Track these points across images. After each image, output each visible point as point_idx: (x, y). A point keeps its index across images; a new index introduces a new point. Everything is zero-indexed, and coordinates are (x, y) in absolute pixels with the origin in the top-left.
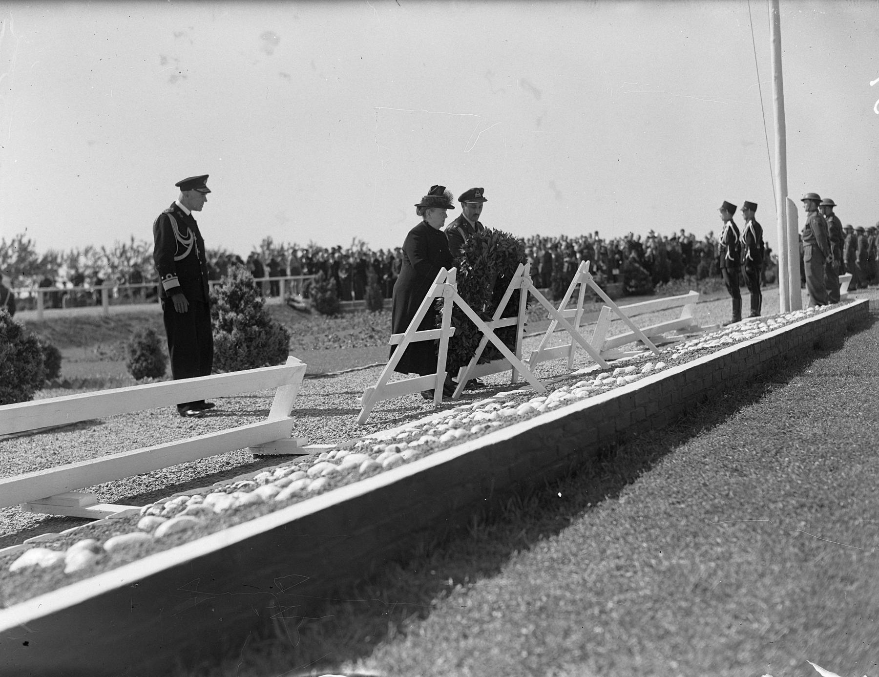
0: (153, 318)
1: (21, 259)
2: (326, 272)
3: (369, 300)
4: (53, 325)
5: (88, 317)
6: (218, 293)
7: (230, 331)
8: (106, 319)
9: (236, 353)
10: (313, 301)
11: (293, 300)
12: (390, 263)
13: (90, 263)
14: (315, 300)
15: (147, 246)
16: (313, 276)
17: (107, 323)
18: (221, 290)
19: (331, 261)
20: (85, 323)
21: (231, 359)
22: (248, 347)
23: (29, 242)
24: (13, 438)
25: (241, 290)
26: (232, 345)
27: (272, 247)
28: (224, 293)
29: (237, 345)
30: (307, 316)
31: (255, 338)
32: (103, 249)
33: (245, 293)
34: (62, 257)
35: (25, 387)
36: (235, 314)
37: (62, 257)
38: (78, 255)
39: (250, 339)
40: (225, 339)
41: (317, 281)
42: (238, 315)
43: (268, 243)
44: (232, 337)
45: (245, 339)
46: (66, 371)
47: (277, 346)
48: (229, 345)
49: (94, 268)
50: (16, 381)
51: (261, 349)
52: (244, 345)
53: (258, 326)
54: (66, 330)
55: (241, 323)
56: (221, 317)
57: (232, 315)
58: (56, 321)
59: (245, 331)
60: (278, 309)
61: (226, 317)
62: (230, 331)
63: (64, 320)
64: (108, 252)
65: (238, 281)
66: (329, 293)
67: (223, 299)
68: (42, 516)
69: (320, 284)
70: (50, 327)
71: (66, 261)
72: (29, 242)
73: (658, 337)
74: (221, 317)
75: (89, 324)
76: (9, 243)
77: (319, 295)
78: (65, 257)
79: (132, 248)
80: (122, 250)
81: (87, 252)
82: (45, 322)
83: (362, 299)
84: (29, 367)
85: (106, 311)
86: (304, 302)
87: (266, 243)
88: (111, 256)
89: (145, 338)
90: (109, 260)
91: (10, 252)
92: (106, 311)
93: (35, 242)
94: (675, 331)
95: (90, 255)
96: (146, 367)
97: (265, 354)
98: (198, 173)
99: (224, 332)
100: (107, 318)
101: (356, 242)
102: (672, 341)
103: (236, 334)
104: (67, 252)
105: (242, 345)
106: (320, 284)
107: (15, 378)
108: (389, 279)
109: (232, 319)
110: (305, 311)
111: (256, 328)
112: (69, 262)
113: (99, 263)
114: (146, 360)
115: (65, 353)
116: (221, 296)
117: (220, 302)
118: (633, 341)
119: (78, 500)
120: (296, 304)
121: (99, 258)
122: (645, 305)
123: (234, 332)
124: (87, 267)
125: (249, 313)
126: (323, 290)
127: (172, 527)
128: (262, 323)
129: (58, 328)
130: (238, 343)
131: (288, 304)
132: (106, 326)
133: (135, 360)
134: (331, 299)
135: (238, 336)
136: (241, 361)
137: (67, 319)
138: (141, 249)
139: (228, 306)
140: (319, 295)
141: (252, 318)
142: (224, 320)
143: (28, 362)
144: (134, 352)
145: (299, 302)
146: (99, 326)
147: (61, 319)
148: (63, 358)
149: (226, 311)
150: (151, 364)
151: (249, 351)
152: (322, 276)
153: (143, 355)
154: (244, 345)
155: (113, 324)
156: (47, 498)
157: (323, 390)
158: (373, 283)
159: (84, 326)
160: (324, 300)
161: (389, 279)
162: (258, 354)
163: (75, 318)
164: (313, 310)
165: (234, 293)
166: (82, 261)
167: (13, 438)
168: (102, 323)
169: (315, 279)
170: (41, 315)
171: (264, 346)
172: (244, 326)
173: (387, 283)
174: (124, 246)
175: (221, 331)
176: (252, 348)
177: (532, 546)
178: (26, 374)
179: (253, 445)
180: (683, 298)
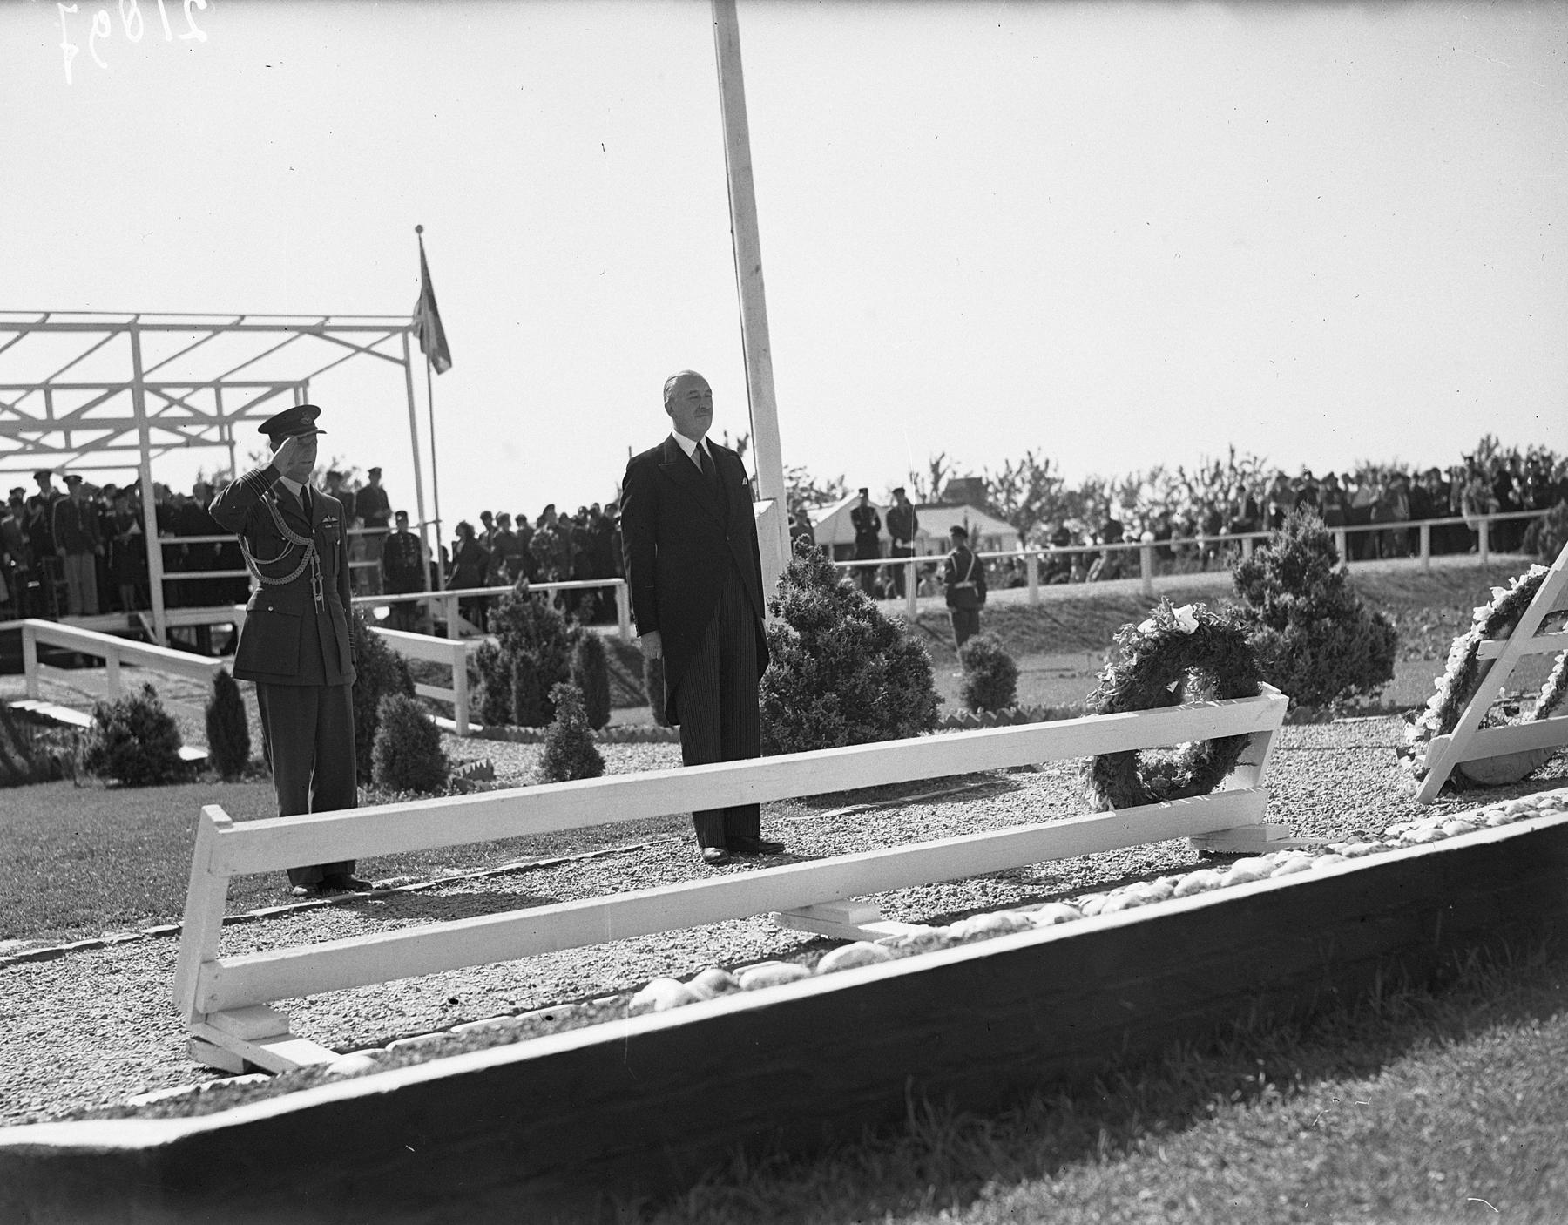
1: (1035, 495)
4: (1054, 611)
5: (1117, 598)
6: (1263, 559)
7: (1280, 627)
9: (1292, 667)
13: (1160, 497)
15: (1258, 463)
16: (1546, 512)
18: (1268, 554)
20: (1111, 608)
21: (1283, 676)
22: (1313, 655)
23: (1047, 463)
24: (872, 809)
25: (1303, 554)
26: (1283, 652)
27: (1497, 452)
28: (1274, 560)
29: (1293, 651)
31: (1326, 640)
32: (1181, 470)
33: (1309, 560)
34: (1112, 488)
35: (900, 726)
36: (1292, 597)
37: (1112, 488)
38: (1140, 484)
39: (1316, 643)
40: (1272, 640)
42: (1297, 598)
43: (1487, 446)
44: (1284, 638)
45: (1310, 641)
46: (1026, 693)
47: (1369, 654)
48: (1278, 652)
49: (1166, 505)
50: (887, 715)
51: (1337, 660)
52: (1307, 652)
53: (1332, 618)
54: (1077, 621)
55: (1303, 613)
56: (1267, 602)
57: (1287, 598)
58: (1059, 605)
59: (1308, 625)
60: (1475, 575)
61: (1276, 602)
62: (1280, 627)
63: (1074, 603)
65: (1299, 538)
67: (1272, 570)
68: (806, 937)
70: (1049, 616)
71: (1118, 494)
72: (1047, 463)
74: (1267, 602)
75: (1117, 609)
76: (1015, 467)
78: (1118, 488)
79: (1232, 467)
80: (1213, 471)
81: (1154, 477)
82: (1041, 607)
84: (909, 693)
85: (1148, 586)
88: (1193, 484)
90: (1191, 489)
91: (1018, 483)
92: (1148, 586)
95: (1158, 482)
97: (1344, 668)
99: (1271, 630)
100: (1149, 598)
103: (1291, 632)
105: (1302, 652)
107: (885, 713)
111: (1328, 621)
112: (1122, 496)
113: (1175, 495)
115: (1023, 664)
116: (1268, 565)
117: (1268, 575)
119: (846, 914)
121: (1174, 488)
123: (1289, 627)
124: (1155, 503)
125: (1316, 595)
127: (839, 959)
128: (1338, 613)
129: (1063, 618)
130: (1296, 649)
135: (1296, 634)
136: (1302, 680)
137: (1078, 600)
139: (1279, 582)
141: (1321, 603)
142: (1272, 605)
143: (906, 686)
147: (1069, 601)
148: (1019, 674)
149: (1277, 592)
151: (1315, 663)
154: (1307, 652)
156: (807, 907)
157: (1369, 741)
159: (1108, 614)
162: (1332, 668)
163: (1093, 598)
165: (1290, 560)
166: (1147, 494)
167: (872, 809)
168: (1139, 607)
169: (1550, 517)
170: (1035, 593)
171: (1342, 653)
172: (1307, 618)
175: (1266, 628)
176: (1320, 659)
177: (1470, 1035)
178: (902, 705)
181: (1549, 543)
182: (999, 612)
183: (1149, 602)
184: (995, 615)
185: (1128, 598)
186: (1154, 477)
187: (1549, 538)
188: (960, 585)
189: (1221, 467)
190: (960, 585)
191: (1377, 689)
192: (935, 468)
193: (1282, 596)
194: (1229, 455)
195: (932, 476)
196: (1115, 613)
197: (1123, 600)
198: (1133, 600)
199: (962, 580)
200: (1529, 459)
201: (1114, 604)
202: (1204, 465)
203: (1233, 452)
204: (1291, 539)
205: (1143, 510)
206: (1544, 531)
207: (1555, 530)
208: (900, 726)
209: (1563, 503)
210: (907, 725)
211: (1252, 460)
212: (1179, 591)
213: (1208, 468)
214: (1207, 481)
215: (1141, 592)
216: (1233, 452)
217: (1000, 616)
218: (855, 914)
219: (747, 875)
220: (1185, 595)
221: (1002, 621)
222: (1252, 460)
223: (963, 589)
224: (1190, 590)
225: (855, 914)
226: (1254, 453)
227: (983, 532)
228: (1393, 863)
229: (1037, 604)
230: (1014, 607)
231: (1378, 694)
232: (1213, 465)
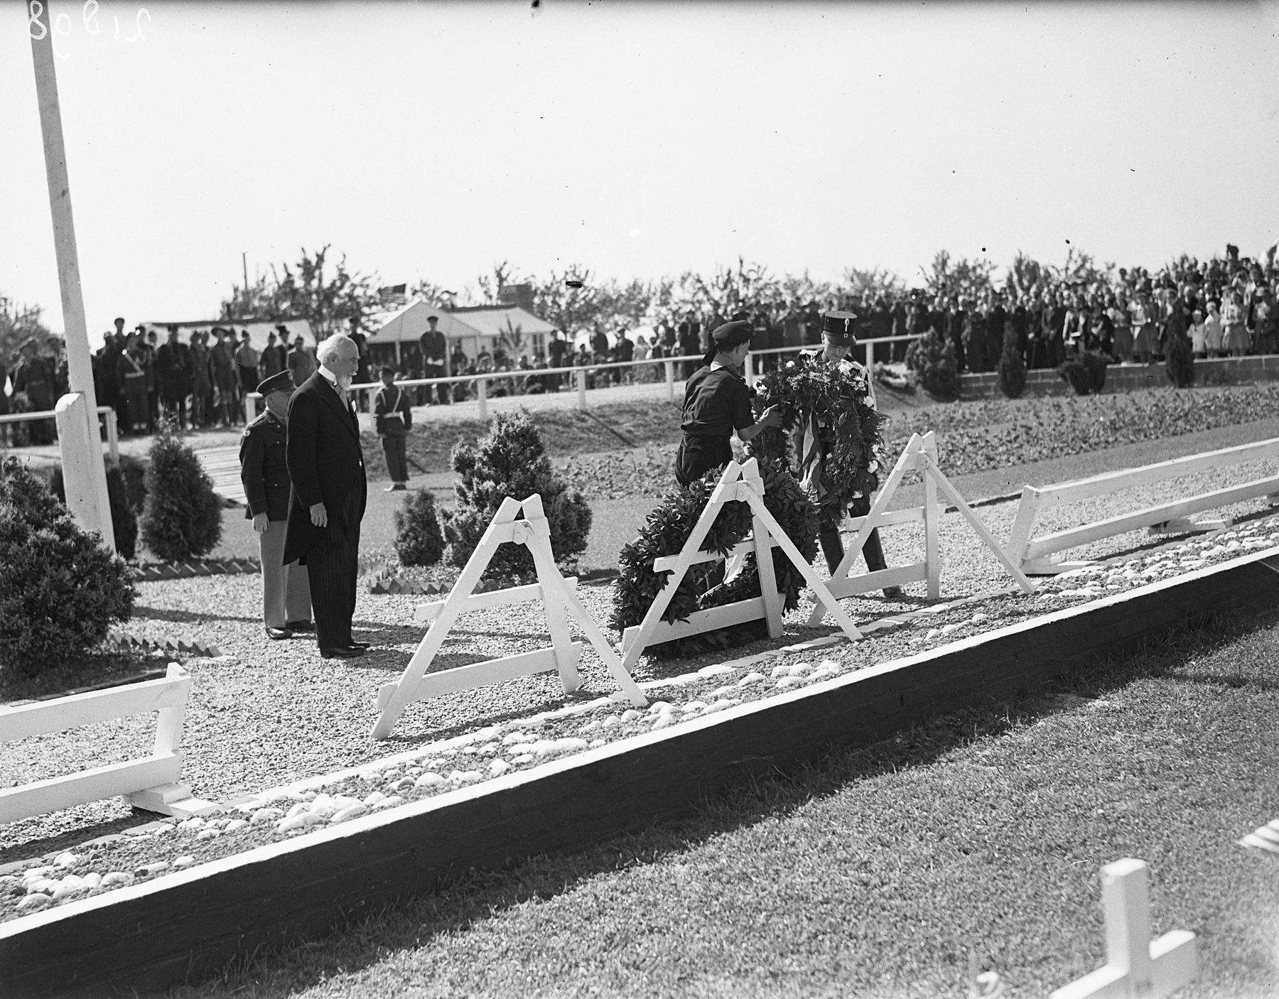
0: (655, 410)
2: (940, 331)
3: (1004, 373)
8: (582, 415)
10: (919, 375)
11: (889, 374)
12: (1039, 314)
13: (688, 297)
14: (922, 373)
15: (761, 270)
16: (919, 336)
17: (583, 420)
19: (953, 311)
20: (549, 422)
25: (505, 446)
30: (908, 398)
35: (84, 624)
41: (925, 343)
56: (475, 488)
64: (707, 282)
66: (943, 361)
69: (930, 348)
73: (1182, 521)
75: (555, 422)
76: (560, 276)
77: (928, 365)
80: (726, 278)
81: (684, 279)
83: (992, 370)
86: (906, 376)
87: (940, 260)
88: (709, 288)
89: (417, 505)
93: (595, 273)
94: (1265, 498)
96: (415, 548)
98: (268, 335)
101: (1075, 256)
102: (1202, 529)
104: (657, 285)
106: (930, 348)
108: (1037, 340)
109: (487, 491)
110: (907, 390)
114: (416, 538)
117: (478, 465)
118: (1262, 495)
120: (891, 380)
122: (1094, 483)
124: (684, 301)
126: (934, 357)
131: (879, 380)
132: (580, 424)
133: (402, 536)
134: (945, 371)
138: (753, 276)
140: (928, 365)
144: (401, 524)
145: (898, 377)
146: (568, 426)
150: (422, 543)
152: (933, 334)
153: (412, 529)
155: (590, 422)
158: (1010, 346)
160: (935, 373)
161: (1037, 340)
164: (919, 388)
165: (496, 449)
166: (677, 294)
168: (574, 420)
173: (1034, 345)
174: (729, 274)
179: (127, 793)
180: (1262, 447)
181: (921, 362)
182: (452, 427)
183: (583, 416)
184: (449, 429)
185: (565, 413)
186: (684, 279)
187: (921, 357)
188: (389, 415)
189: (732, 275)
190: (389, 415)
191: (573, 556)
192: (499, 274)
193: (485, 484)
194: (739, 264)
195: (497, 280)
196: (553, 426)
197: (561, 414)
198: (569, 415)
199: (391, 411)
200: (931, 286)
201: (551, 418)
202: (719, 273)
203: (741, 262)
204: (497, 433)
205: (675, 308)
206: (918, 351)
207: (926, 351)
208: (84, 624)
209: (932, 329)
210: (90, 623)
211: (756, 269)
212: (610, 406)
213: (722, 275)
214: (721, 286)
215: (578, 408)
216: (741, 262)
217: (454, 431)
218: (168, 795)
219: (1077, 484)
220: (616, 408)
221: (454, 435)
222: (756, 269)
223: (391, 419)
224: (620, 405)
225: (168, 795)
226: (758, 264)
227: (524, 330)
228: (831, 692)
229: (486, 420)
230: (466, 422)
231: (575, 561)
232: (725, 272)
